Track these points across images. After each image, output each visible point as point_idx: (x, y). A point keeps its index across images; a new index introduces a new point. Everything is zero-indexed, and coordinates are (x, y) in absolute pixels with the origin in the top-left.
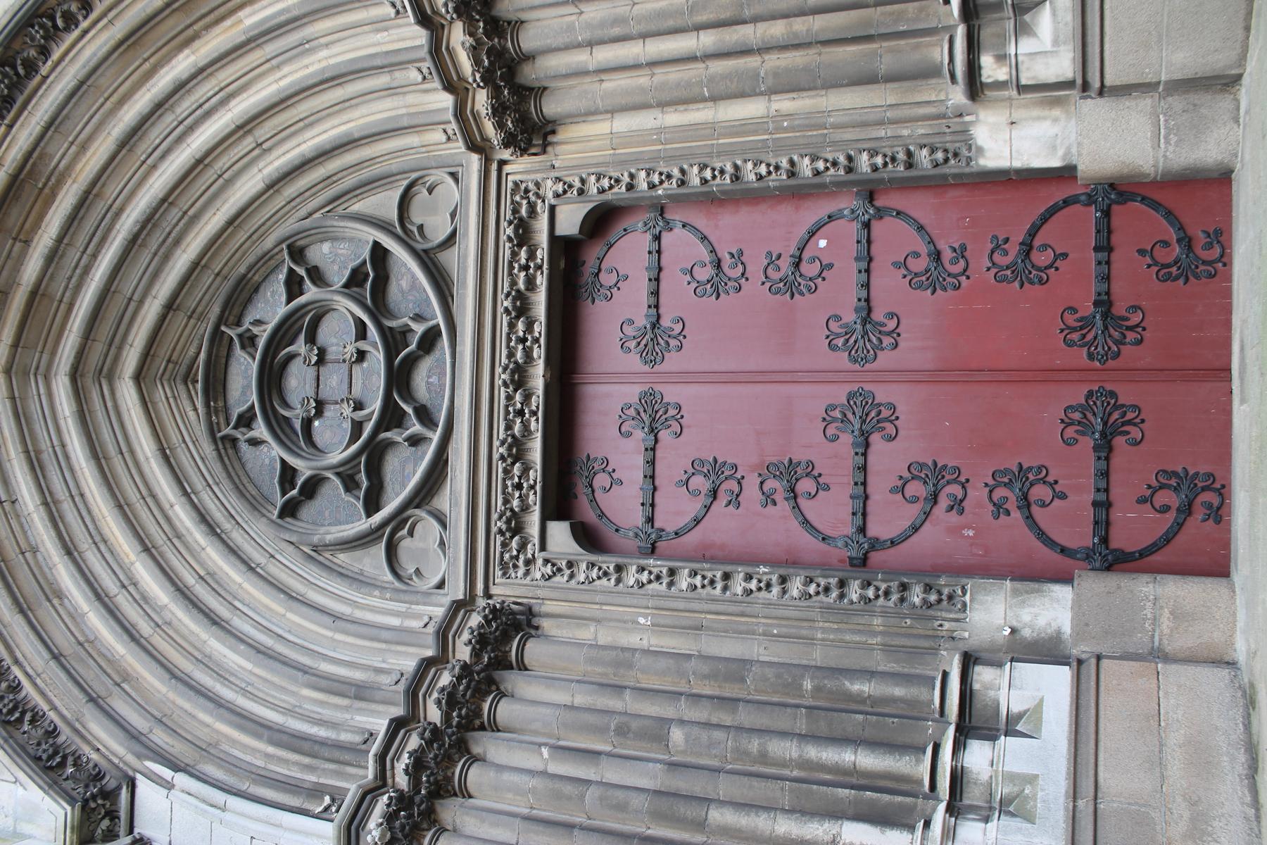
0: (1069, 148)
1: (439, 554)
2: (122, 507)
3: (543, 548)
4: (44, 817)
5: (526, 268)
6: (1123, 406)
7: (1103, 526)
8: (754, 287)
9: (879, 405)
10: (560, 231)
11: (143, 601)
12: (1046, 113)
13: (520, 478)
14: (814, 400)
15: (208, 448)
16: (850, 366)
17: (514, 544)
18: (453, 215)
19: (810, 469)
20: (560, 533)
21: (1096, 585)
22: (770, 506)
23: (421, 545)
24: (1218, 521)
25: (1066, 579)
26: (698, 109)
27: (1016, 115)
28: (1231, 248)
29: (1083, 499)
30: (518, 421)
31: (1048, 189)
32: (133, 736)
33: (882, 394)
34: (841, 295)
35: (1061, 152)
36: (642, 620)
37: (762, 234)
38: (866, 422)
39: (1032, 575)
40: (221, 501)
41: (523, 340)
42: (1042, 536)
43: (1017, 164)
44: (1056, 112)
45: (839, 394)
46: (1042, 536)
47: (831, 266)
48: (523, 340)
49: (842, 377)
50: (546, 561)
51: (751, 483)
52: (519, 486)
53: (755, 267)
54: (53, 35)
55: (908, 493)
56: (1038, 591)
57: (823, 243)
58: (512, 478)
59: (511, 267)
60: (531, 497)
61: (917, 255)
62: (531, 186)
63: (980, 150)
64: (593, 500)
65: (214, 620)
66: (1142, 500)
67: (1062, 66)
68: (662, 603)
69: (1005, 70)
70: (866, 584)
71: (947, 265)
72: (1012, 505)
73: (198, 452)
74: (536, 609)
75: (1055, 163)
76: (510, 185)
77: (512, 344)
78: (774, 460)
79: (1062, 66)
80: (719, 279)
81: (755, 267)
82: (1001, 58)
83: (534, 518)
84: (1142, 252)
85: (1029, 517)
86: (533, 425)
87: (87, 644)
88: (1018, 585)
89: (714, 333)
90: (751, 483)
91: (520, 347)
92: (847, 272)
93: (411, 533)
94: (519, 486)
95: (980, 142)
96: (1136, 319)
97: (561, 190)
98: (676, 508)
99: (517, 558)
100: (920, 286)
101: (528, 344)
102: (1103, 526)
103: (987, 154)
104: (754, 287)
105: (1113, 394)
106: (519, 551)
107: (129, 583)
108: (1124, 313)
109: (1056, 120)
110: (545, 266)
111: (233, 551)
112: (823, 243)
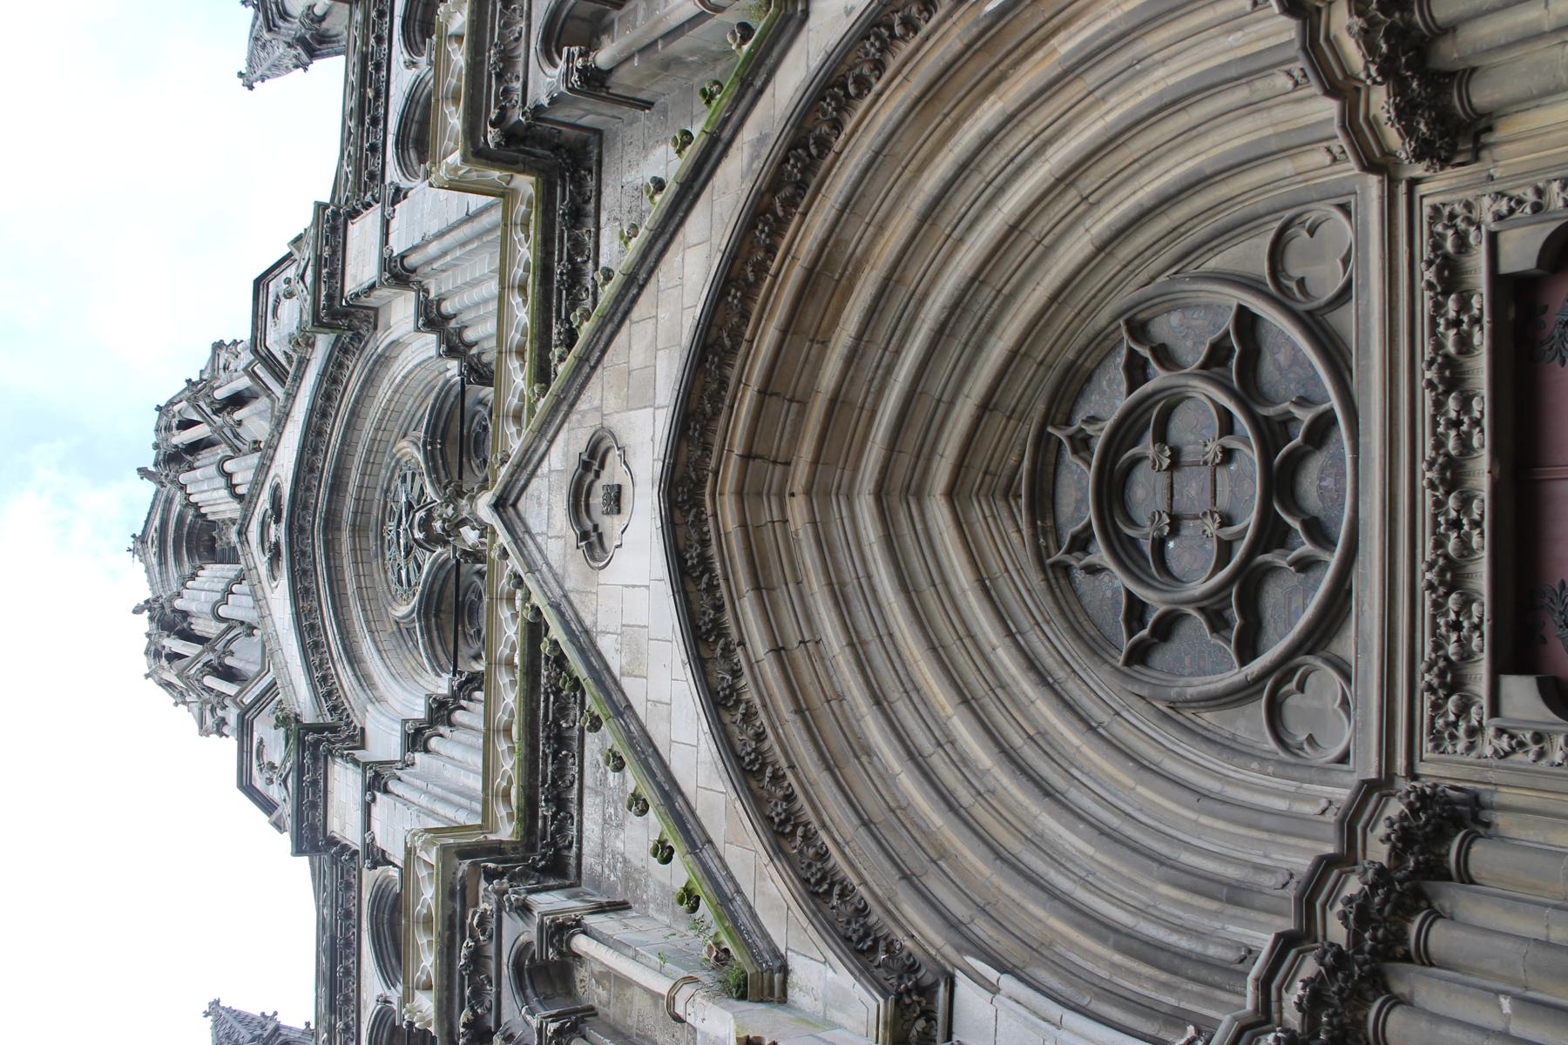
1: (1342, 716)
2: (936, 649)
3: (1495, 710)
5: (1457, 323)
10: (1508, 265)
11: (962, 762)
15: (1036, 579)
17: (1451, 704)
18: (1346, 261)
20: (1521, 694)
32: (952, 924)
40: (1053, 642)
41: (1457, 424)
48: (1457, 424)
50: (1500, 732)
58: (1446, 614)
59: (1434, 324)
60: (1476, 641)
62: (1459, 209)
65: (1046, 791)
73: (1024, 583)
74: (1486, 798)
76: (1427, 211)
83: (1481, 671)
87: (900, 810)
93: (1301, 688)
107: (946, 741)
111: (1069, 706)
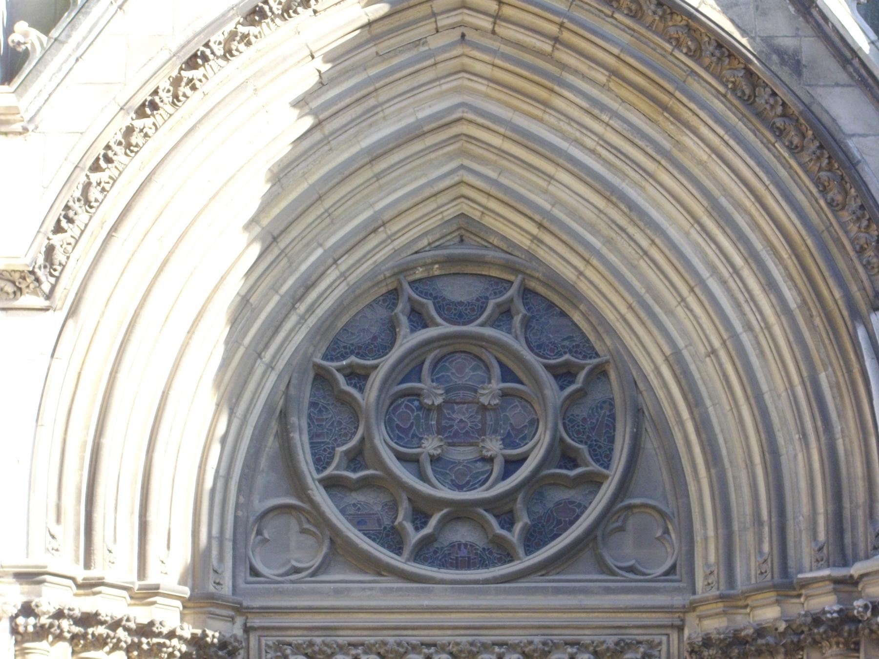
18: (631, 569)
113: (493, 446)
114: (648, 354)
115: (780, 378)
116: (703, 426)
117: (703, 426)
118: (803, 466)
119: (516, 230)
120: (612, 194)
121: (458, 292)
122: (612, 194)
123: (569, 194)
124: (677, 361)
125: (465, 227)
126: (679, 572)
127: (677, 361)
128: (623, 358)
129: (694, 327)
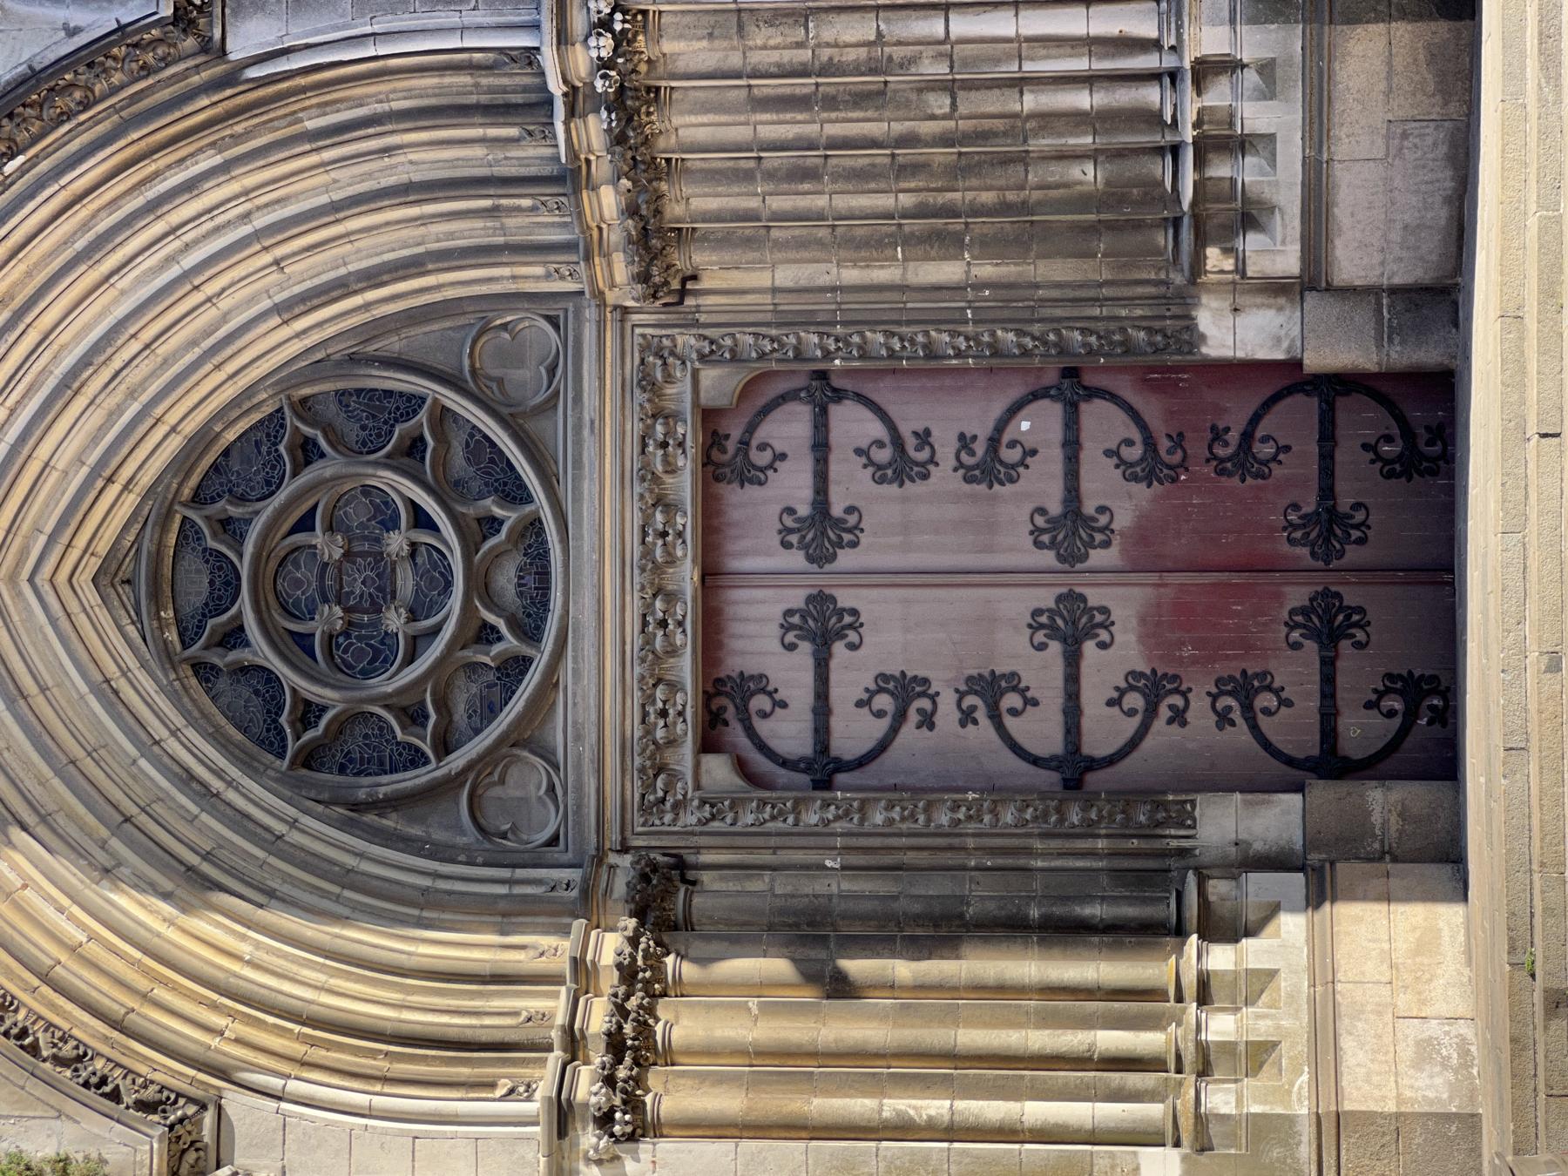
0: (1293, 340)
4: (135, 1150)
6: (1349, 607)
7: (1329, 732)
8: (945, 476)
9: (1093, 609)
10: (705, 400)
12: (1272, 301)
13: (665, 702)
14: (1019, 603)
16: (1059, 566)
19: (1013, 682)
21: (1324, 792)
22: (970, 727)
23: (518, 794)
24: (1444, 724)
25: (1299, 788)
26: (882, 267)
27: (1240, 300)
28: (1454, 445)
29: (1308, 705)
30: (660, 633)
31: (1287, 378)
33: (1095, 597)
34: (1043, 484)
35: (1285, 345)
36: (829, 863)
37: (953, 418)
38: (1072, 627)
39: (1256, 786)
41: (664, 534)
42: (1267, 745)
43: (1240, 354)
44: (1282, 301)
45: (1045, 598)
46: (1267, 745)
47: (1034, 452)
49: (1049, 578)
51: (947, 702)
52: (663, 714)
53: (946, 451)
54: (827, 665)
55: (1019, 449)
56: (1263, 802)
57: (1025, 426)
58: (654, 702)
60: (680, 727)
61: (1129, 443)
63: (1203, 338)
64: (750, 732)
66: (1369, 705)
67: (1288, 262)
68: (854, 842)
69: (1232, 261)
70: (1085, 809)
71: (1163, 453)
72: (1236, 715)
74: (691, 859)
75: (1280, 355)
77: (649, 539)
78: (974, 672)
79: (1288, 262)
80: (902, 464)
81: (946, 451)
82: (1227, 251)
83: (688, 748)
84: (1365, 447)
85: (1254, 728)
86: (679, 639)
88: (1249, 797)
89: (897, 525)
90: (947, 702)
91: (660, 542)
92: (1051, 461)
94: (663, 714)
95: (1202, 328)
96: (1359, 516)
97: (707, 350)
98: (853, 731)
99: (663, 801)
100: (1135, 478)
101: (670, 538)
102: (1329, 732)
103: (1210, 342)
104: (945, 476)
105: (1338, 595)
106: (666, 793)
108: (1307, 643)
109: (1280, 309)
110: (689, 443)
112: (1025, 426)
113: (396, 542)
114: (277, 346)
115: (312, 180)
116: (373, 277)
117: (373, 277)
118: (426, 154)
119: (114, 512)
120: (69, 384)
121: (197, 585)
122: (69, 384)
123: (70, 442)
124: (287, 309)
125: (109, 576)
126: (556, 311)
127: (287, 309)
128: (285, 378)
129: (247, 286)
